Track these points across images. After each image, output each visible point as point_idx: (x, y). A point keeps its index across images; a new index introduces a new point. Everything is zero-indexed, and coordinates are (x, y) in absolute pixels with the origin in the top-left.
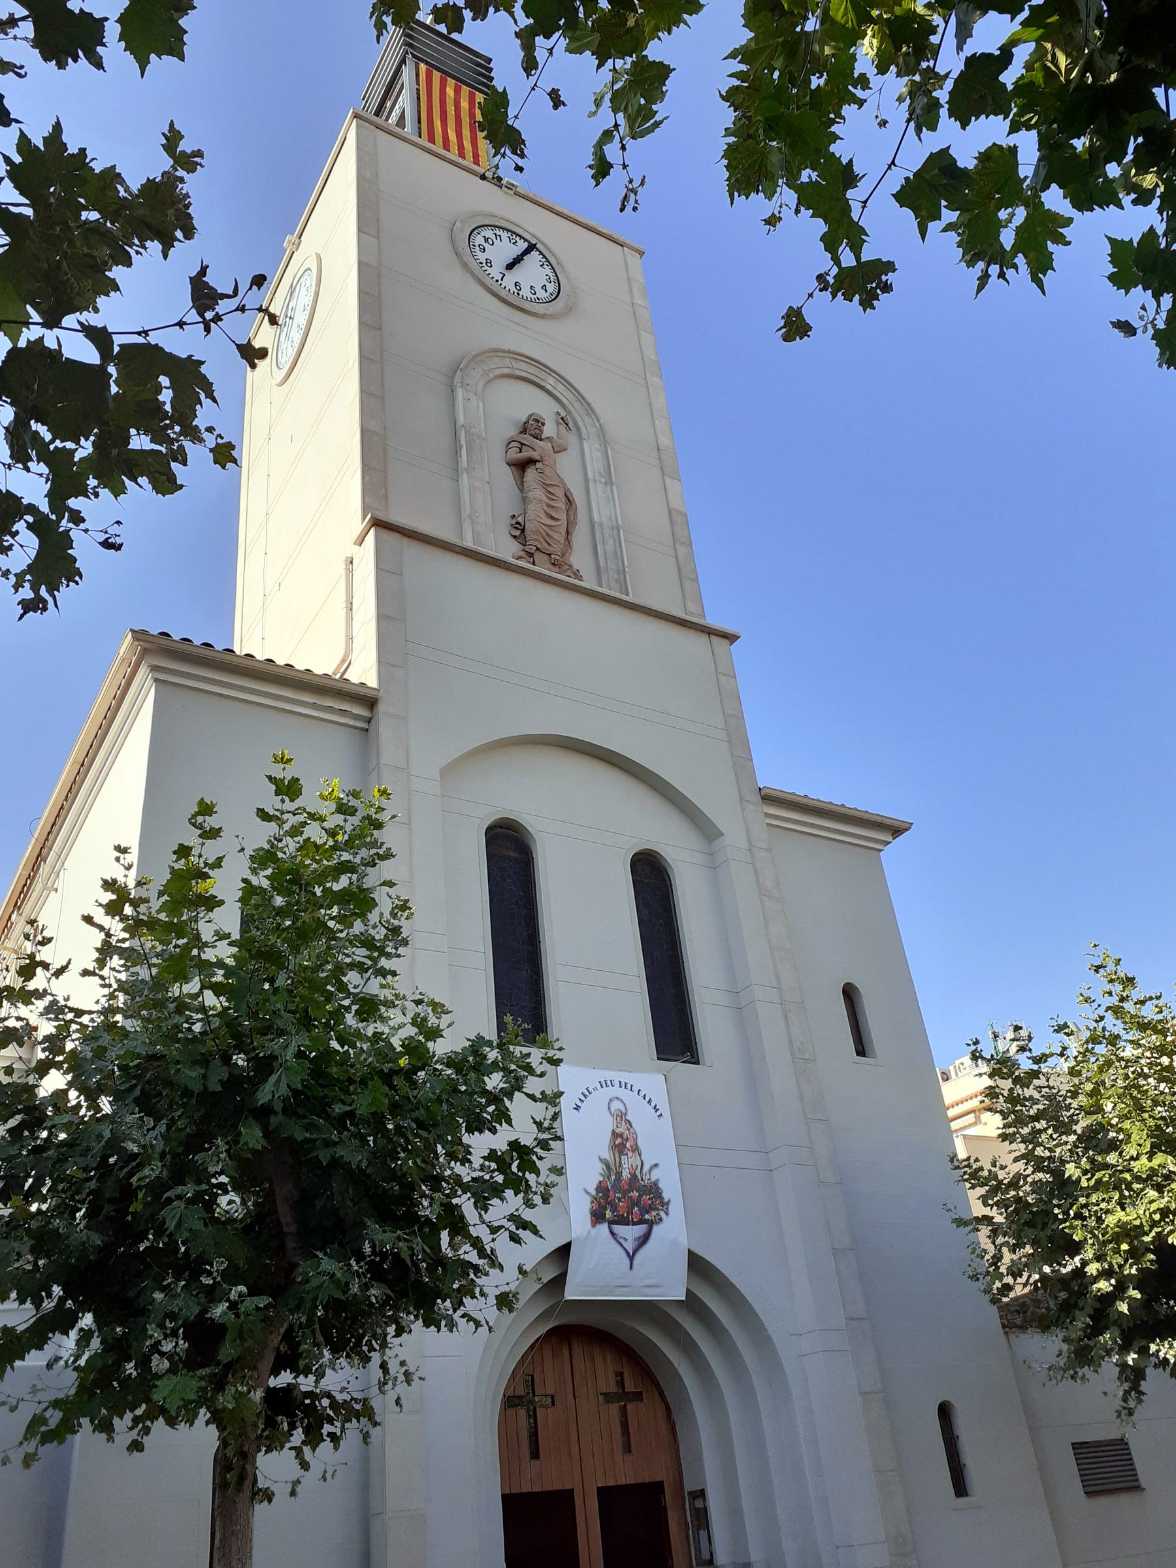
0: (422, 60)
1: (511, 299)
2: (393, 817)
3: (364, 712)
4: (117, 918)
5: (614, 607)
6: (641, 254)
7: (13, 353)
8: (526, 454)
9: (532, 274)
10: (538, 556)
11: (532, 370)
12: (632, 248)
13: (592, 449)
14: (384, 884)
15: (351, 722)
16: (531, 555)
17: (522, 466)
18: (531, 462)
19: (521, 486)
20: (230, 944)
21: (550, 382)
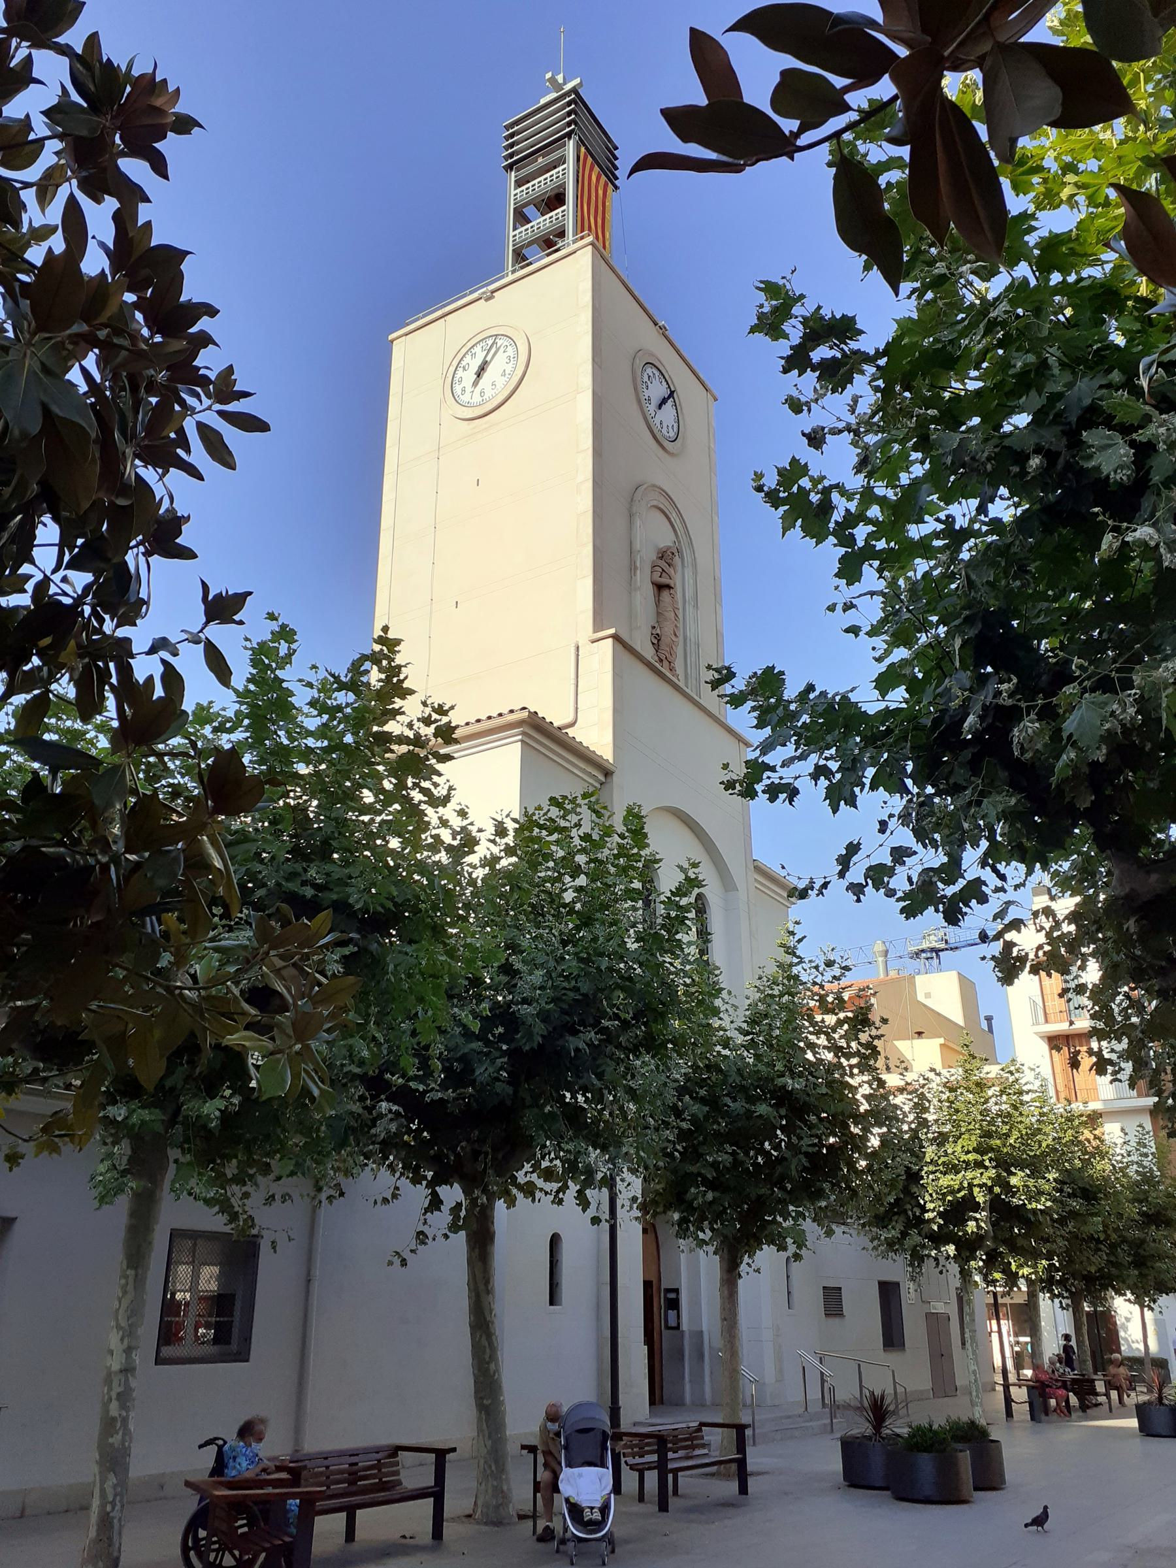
0: (584, 145)
1: (656, 431)
2: (783, 867)
3: (602, 778)
4: (882, 891)
5: (715, 724)
6: (716, 400)
7: (57, 164)
8: (665, 580)
9: (667, 414)
10: (665, 663)
11: (667, 504)
12: (712, 395)
13: (688, 573)
14: (1023, 885)
15: (591, 781)
16: (661, 661)
17: (660, 587)
18: (669, 587)
19: (658, 602)
20: (898, 900)
21: (674, 516)
